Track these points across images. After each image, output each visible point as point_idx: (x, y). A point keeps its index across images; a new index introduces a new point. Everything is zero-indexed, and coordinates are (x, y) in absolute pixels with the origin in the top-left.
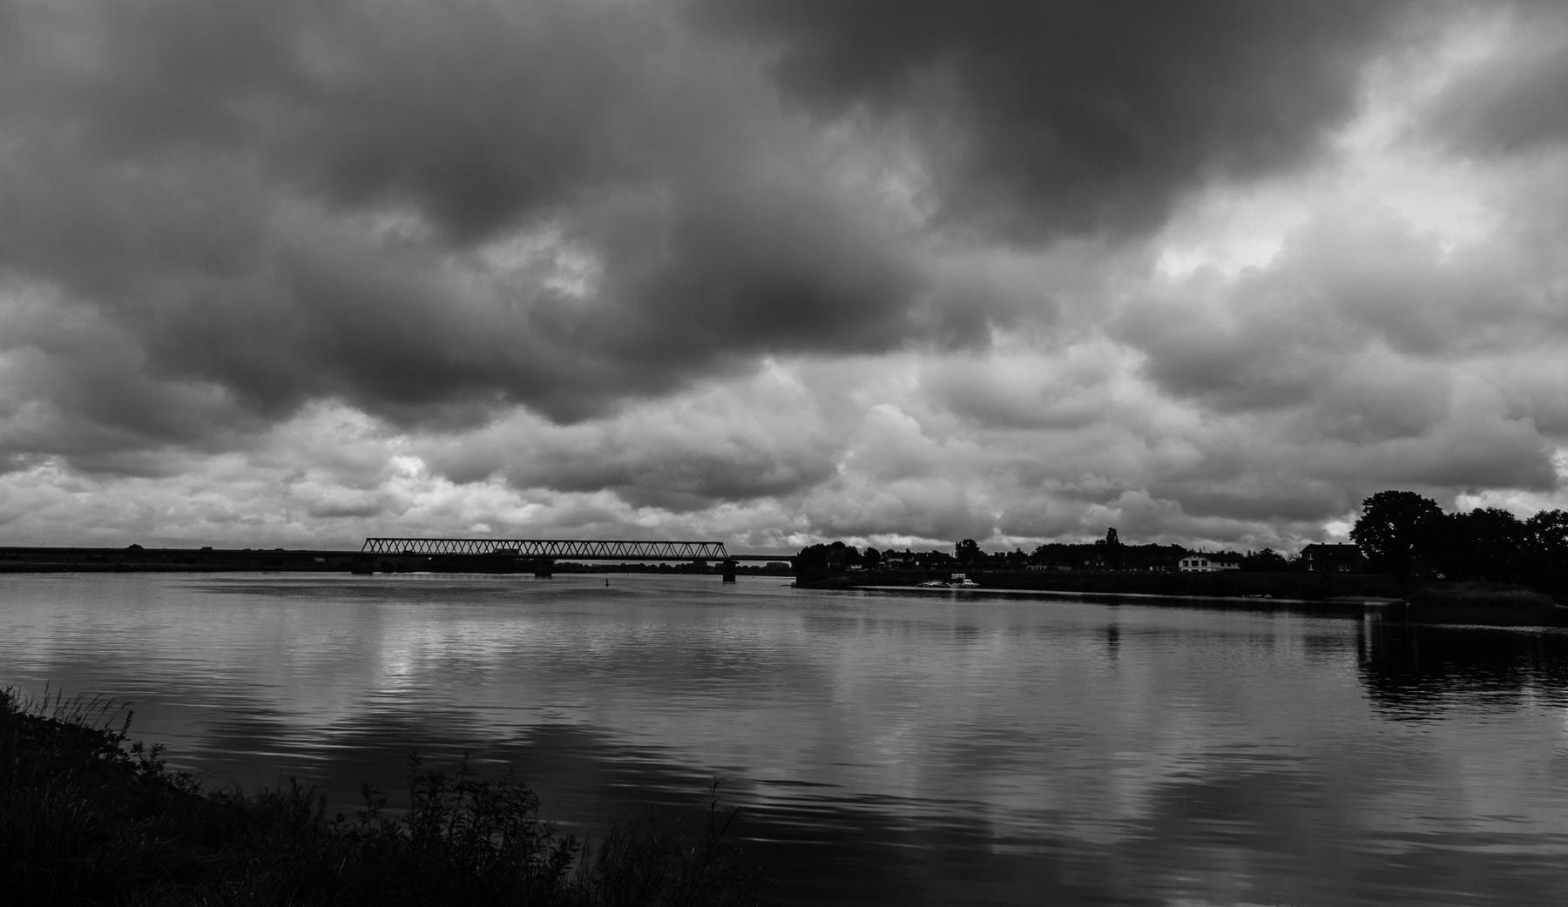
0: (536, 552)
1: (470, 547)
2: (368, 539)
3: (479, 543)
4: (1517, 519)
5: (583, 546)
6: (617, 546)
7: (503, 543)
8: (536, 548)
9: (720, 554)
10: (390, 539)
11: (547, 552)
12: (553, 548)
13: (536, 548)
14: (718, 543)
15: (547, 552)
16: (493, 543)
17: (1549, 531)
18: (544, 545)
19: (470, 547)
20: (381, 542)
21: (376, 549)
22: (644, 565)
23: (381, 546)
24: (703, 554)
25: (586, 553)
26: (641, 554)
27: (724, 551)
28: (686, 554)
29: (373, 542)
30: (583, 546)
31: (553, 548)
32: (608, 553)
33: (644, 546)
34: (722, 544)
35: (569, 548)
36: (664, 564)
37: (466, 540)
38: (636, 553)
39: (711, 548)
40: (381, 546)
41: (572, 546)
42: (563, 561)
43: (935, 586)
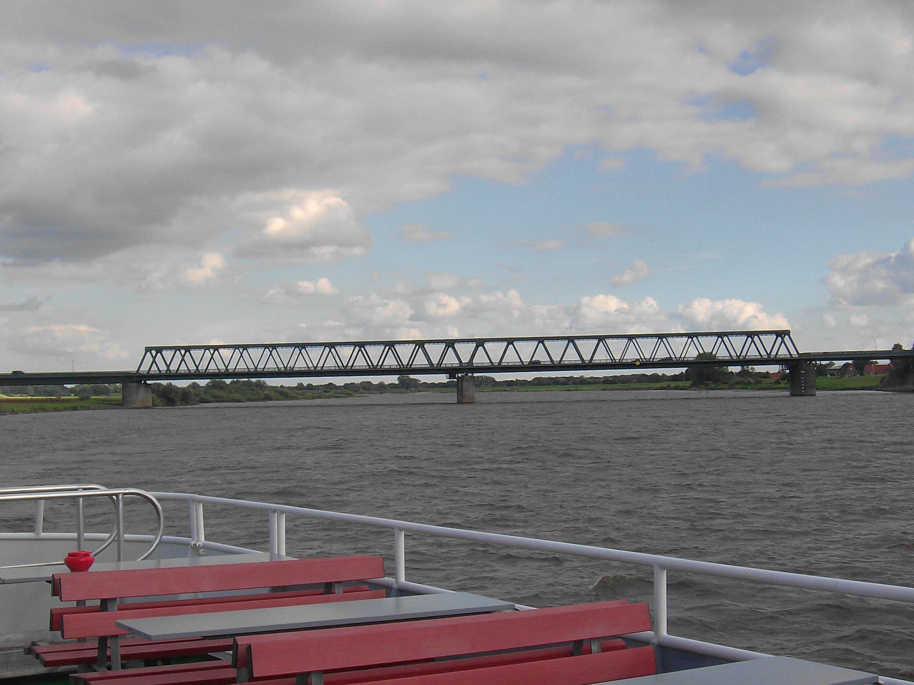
2: (148, 350)
6: (327, 349)
26: (251, 366)
28: (331, 364)
33: (255, 353)
34: (787, 333)
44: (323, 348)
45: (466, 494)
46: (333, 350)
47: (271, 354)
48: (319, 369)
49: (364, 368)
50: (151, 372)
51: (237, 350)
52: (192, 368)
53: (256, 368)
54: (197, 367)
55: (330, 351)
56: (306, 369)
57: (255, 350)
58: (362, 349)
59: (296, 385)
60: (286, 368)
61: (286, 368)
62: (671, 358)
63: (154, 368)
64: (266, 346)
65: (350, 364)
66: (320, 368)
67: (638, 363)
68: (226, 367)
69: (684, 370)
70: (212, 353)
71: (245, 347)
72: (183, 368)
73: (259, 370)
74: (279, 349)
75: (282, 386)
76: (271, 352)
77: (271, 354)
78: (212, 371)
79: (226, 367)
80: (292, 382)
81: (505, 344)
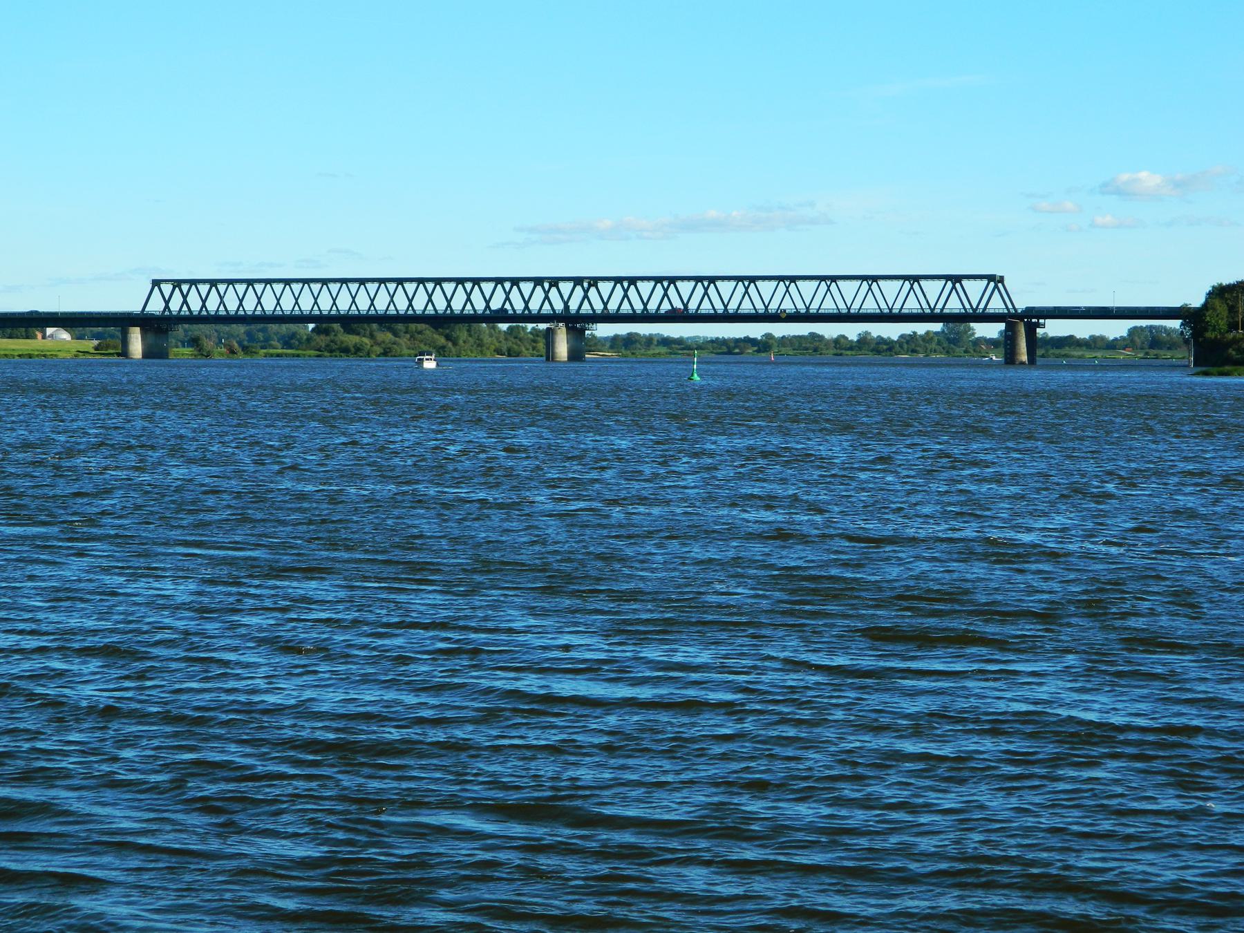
0: (586, 306)
1: (430, 296)
2: (156, 283)
3: (410, 287)
4: (855, 339)
5: (992, 284)
6: (823, 285)
7: (469, 286)
8: (547, 297)
9: (996, 305)
10: (204, 281)
11: (573, 306)
12: (586, 297)
13: (547, 297)
14: (991, 278)
15: (573, 306)
16: (407, 285)
17: (1035, 322)
18: (645, 287)
19: (430, 296)
20: (185, 287)
21: (175, 305)
22: (821, 338)
23: (185, 297)
24: (954, 305)
25: (666, 306)
26: (842, 306)
27: (1007, 296)
28: (912, 305)
29: (469, 286)
30: (950, 284)
31: (586, 297)
32: (883, 306)
33: (807, 287)
34: (1001, 280)
35: (626, 296)
36: (867, 333)
37: (382, 281)
38: (788, 306)
39: (974, 289)
40: (185, 297)
41: (632, 292)
42: (623, 329)
43: (652, 843)
44: (943, 282)
45: (447, 527)
46: (958, 285)
47: (828, 289)
48: (937, 311)
49: (1001, 311)
50: (542, 312)
51: (781, 283)
52: (760, 307)
53: (808, 308)
54: (726, 306)
55: (954, 287)
56: (920, 311)
57: (766, 283)
58: (1000, 285)
59: (806, 333)
60: (891, 310)
61: (808, 308)
62: (798, 312)
63: (547, 306)
64: (864, 278)
65: (982, 306)
66: (981, 311)
67: (784, 316)
68: (766, 307)
69: (937, 327)
70: (626, 287)
71: (793, 279)
72: (626, 308)
73: (811, 311)
74: (799, 283)
75: (889, 338)
76: (870, 286)
77: (828, 289)
78: (746, 312)
79: (766, 307)
80: (852, 331)
81: (612, 284)
